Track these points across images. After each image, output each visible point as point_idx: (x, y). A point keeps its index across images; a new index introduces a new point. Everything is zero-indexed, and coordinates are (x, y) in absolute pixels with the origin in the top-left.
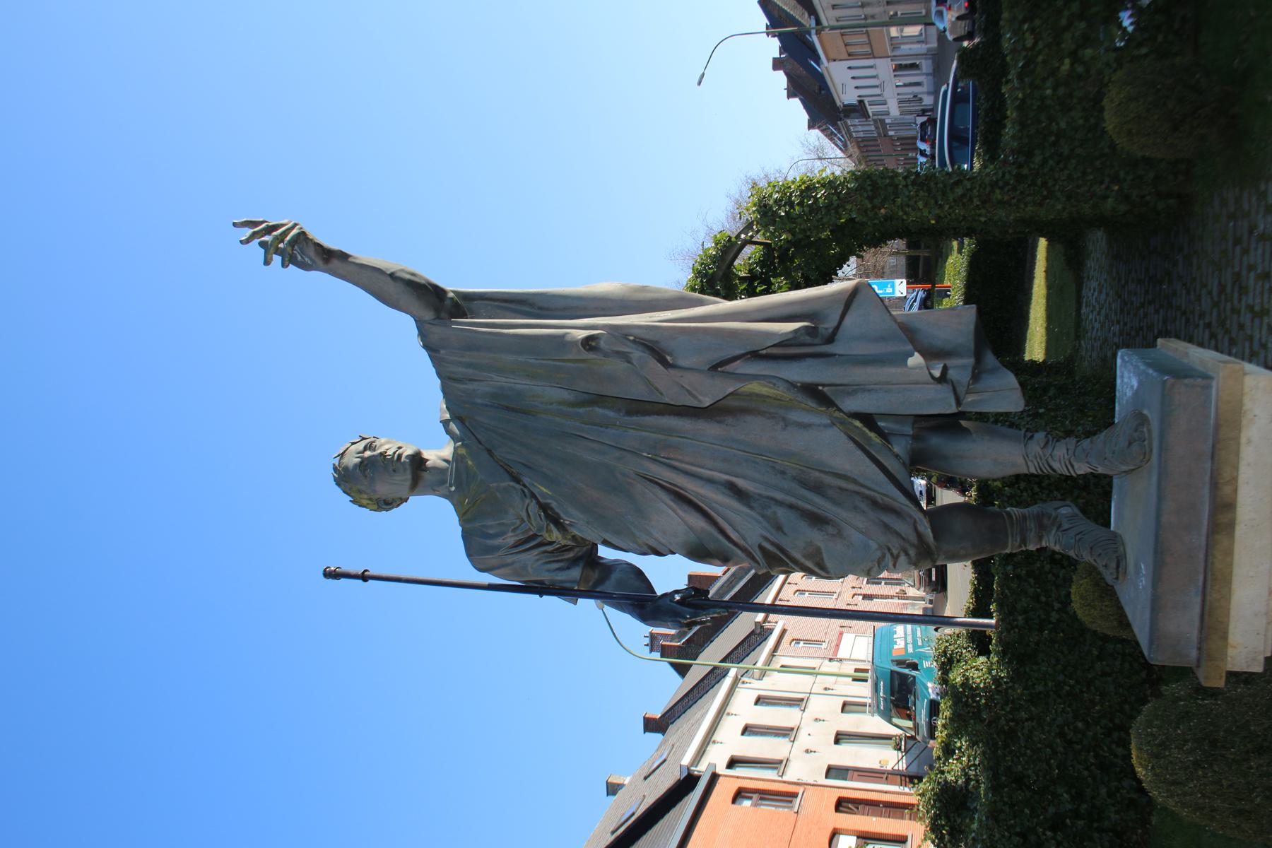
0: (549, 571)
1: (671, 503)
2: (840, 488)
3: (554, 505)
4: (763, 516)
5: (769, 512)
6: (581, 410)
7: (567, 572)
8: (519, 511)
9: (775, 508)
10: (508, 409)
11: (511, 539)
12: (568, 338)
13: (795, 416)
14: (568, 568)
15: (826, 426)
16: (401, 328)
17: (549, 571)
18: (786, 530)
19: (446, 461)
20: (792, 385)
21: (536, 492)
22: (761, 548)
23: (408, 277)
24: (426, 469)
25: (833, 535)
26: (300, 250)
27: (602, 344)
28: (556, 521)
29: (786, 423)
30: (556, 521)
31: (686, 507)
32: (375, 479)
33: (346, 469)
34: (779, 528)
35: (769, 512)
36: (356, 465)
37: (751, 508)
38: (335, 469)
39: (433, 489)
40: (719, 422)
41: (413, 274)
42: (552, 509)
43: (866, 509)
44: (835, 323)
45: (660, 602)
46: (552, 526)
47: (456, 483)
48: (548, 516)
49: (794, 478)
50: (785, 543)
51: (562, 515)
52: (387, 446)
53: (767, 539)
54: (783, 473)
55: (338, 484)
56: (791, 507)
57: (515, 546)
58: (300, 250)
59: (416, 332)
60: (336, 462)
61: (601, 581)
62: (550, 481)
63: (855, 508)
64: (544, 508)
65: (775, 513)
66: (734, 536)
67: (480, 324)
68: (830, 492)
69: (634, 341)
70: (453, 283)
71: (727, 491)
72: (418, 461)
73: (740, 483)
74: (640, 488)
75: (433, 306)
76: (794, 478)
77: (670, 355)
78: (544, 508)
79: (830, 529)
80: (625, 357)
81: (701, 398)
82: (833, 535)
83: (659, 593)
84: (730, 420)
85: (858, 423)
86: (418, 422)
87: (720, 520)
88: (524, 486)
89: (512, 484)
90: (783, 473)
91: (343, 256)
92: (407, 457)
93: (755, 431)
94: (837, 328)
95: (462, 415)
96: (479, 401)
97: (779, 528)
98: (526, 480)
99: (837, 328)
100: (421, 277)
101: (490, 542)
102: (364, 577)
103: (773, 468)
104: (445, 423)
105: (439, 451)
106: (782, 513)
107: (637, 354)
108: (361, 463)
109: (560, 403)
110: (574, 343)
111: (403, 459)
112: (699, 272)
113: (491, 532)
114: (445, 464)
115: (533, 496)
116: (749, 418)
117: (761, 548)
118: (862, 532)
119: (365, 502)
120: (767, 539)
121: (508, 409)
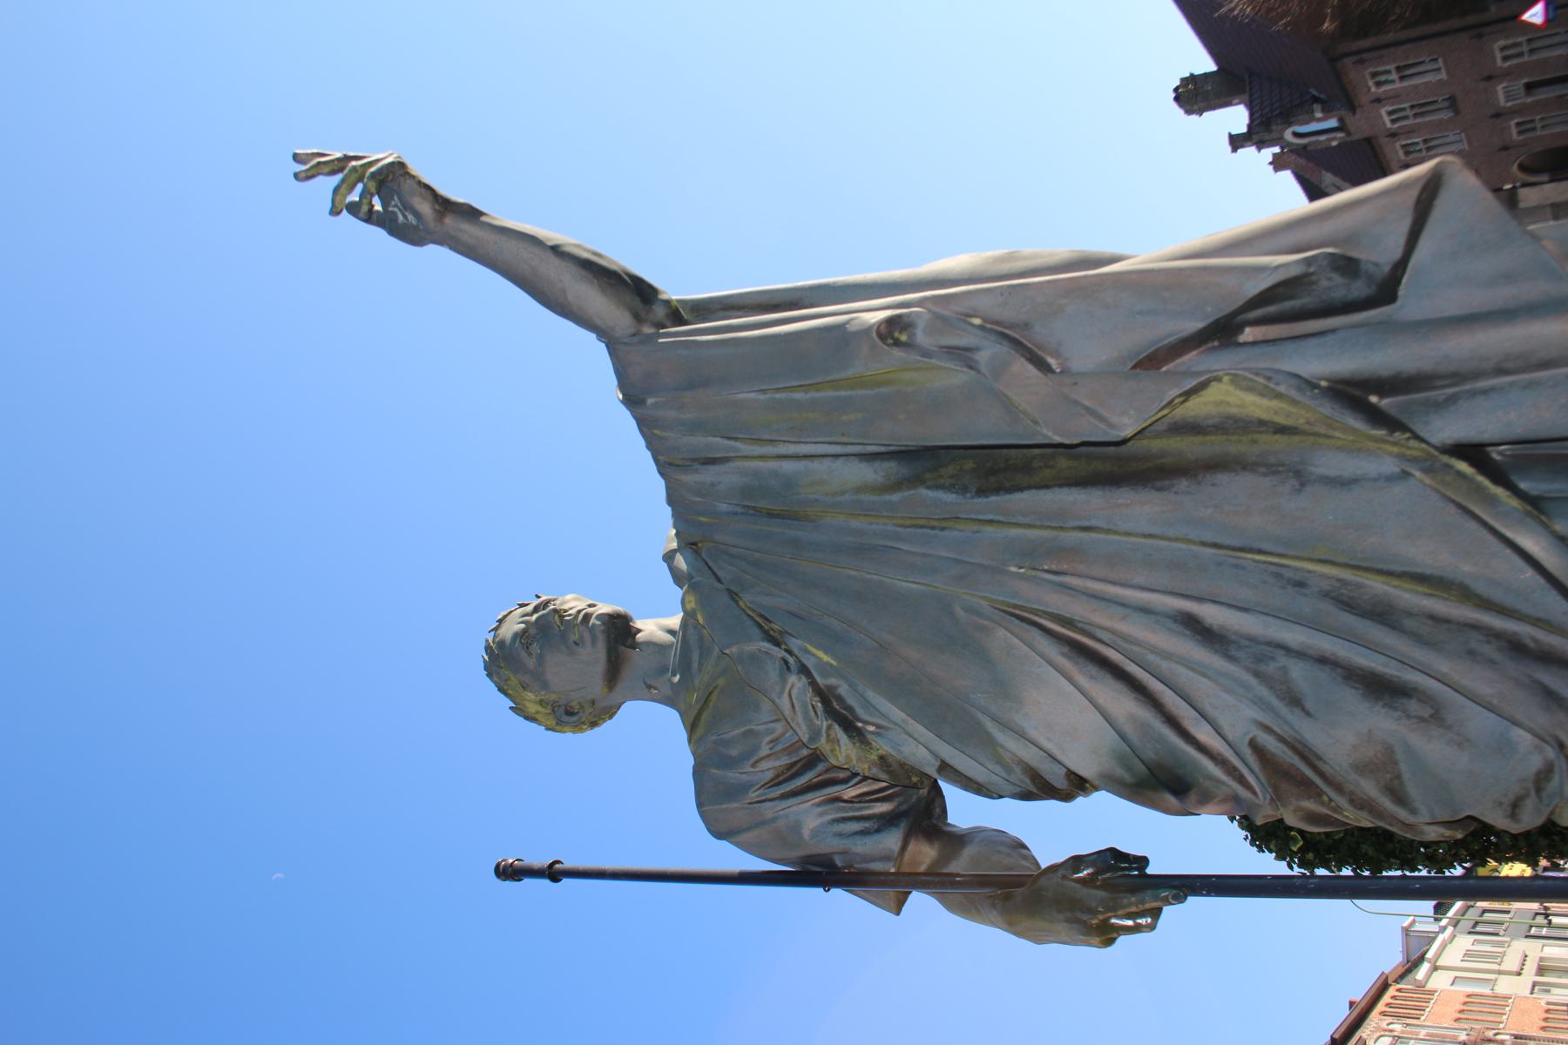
0: (840, 835)
1: (1066, 664)
2: (1435, 618)
3: (843, 690)
4: (1257, 674)
5: (1270, 668)
6: (895, 497)
7: (876, 837)
8: (788, 709)
9: (1283, 660)
10: (771, 515)
11: (769, 769)
12: (852, 328)
13: (1329, 463)
14: (878, 831)
15: (1390, 479)
16: (580, 363)
17: (840, 835)
18: (1309, 705)
19: (671, 632)
20: (1309, 384)
21: (810, 663)
22: (1253, 744)
23: (585, 255)
24: (634, 645)
25: (1422, 719)
26: (395, 200)
27: (921, 338)
28: (849, 724)
29: (1301, 478)
30: (849, 724)
31: (1093, 669)
32: (559, 666)
33: (501, 644)
34: (1295, 701)
35: (1270, 668)
36: (516, 635)
37: (1231, 658)
38: (488, 648)
39: (648, 691)
40: (1159, 489)
41: (599, 255)
42: (840, 699)
43: (1497, 656)
44: (1397, 253)
45: (1043, 882)
46: (838, 732)
47: (704, 685)
48: (830, 712)
49: (1325, 595)
50: (1313, 734)
51: (860, 712)
52: (573, 603)
53: (1267, 729)
54: (1300, 584)
55: (489, 675)
56: (1323, 660)
57: (775, 782)
58: (395, 200)
59: (615, 382)
60: (490, 637)
61: (944, 859)
62: (831, 640)
63: (1471, 653)
64: (826, 697)
65: (1284, 670)
66: (1204, 734)
67: (705, 332)
68: (1409, 623)
69: (981, 327)
70: (674, 289)
71: (1180, 628)
72: (619, 629)
73: (1211, 614)
74: (1003, 638)
75: (623, 306)
76: (1325, 595)
77: (1056, 354)
78: (826, 697)
79: (1413, 706)
80: (963, 355)
81: (1114, 419)
82: (1422, 719)
83: (1044, 865)
84: (1183, 484)
85: (1463, 466)
86: (622, 554)
87: (1154, 685)
88: (789, 652)
89: (766, 645)
90: (1300, 584)
91: (471, 213)
92: (600, 617)
93: (1239, 505)
94: (1401, 265)
95: (702, 552)
96: (723, 507)
97: (1295, 701)
98: (795, 644)
99: (1401, 265)
100: (611, 261)
101: (733, 776)
102: (553, 873)
103: (1279, 576)
104: (669, 557)
105: (658, 620)
106: (1298, 672)
107: (989, 351)
108: (524, 631)
109: (860, 489)
110: (866, 331)
111: (593, 621)
112: (562, 617)
113: (734, 752)
114: (669, 638)
115: (804, 670)
116: (1223, 478)
117: (1253, 744)
118: (1489, 708)
119: (532, 708)
120: (1267, 729)
121: (771, 515)
